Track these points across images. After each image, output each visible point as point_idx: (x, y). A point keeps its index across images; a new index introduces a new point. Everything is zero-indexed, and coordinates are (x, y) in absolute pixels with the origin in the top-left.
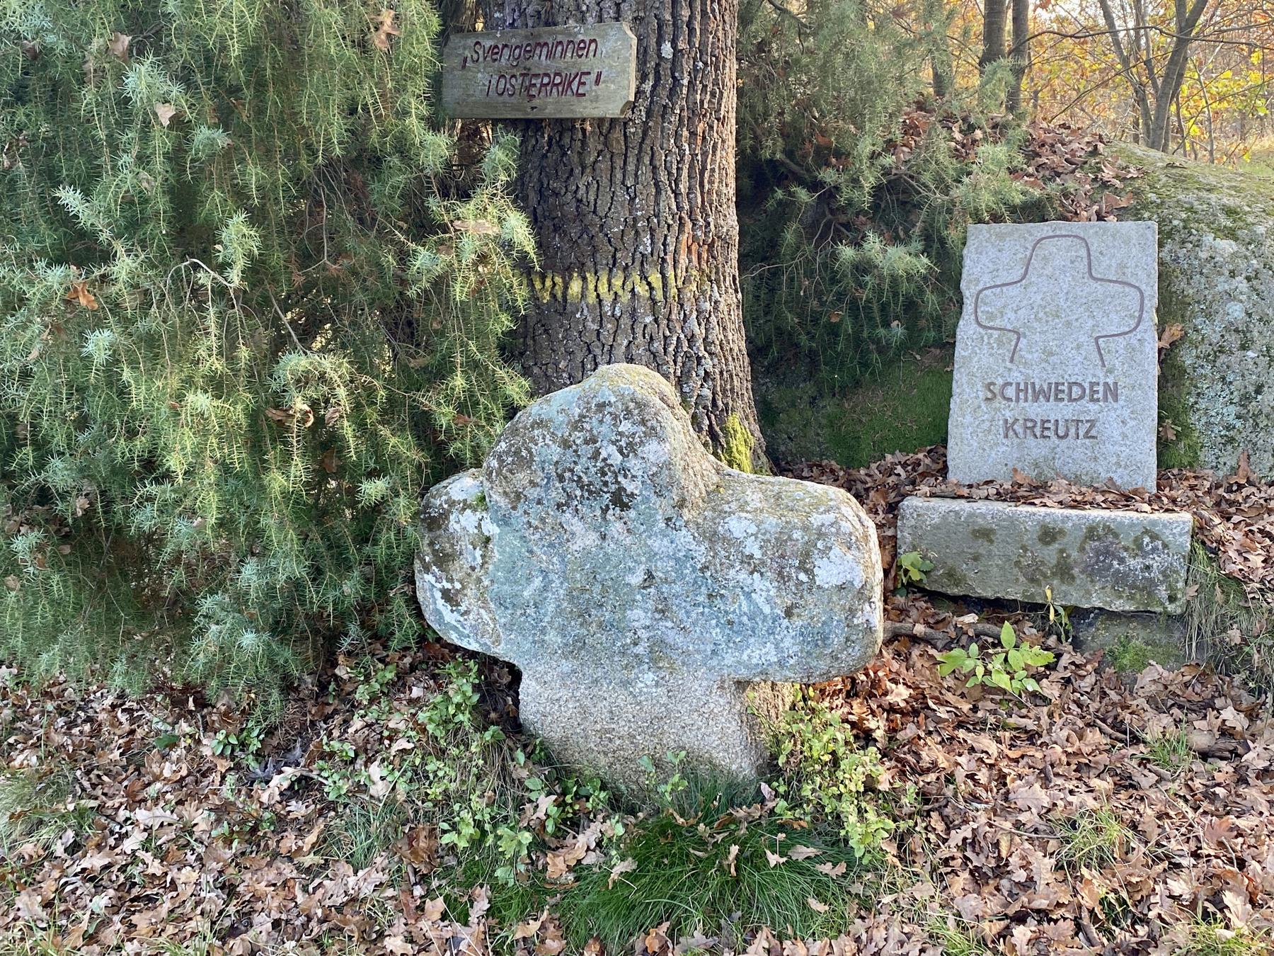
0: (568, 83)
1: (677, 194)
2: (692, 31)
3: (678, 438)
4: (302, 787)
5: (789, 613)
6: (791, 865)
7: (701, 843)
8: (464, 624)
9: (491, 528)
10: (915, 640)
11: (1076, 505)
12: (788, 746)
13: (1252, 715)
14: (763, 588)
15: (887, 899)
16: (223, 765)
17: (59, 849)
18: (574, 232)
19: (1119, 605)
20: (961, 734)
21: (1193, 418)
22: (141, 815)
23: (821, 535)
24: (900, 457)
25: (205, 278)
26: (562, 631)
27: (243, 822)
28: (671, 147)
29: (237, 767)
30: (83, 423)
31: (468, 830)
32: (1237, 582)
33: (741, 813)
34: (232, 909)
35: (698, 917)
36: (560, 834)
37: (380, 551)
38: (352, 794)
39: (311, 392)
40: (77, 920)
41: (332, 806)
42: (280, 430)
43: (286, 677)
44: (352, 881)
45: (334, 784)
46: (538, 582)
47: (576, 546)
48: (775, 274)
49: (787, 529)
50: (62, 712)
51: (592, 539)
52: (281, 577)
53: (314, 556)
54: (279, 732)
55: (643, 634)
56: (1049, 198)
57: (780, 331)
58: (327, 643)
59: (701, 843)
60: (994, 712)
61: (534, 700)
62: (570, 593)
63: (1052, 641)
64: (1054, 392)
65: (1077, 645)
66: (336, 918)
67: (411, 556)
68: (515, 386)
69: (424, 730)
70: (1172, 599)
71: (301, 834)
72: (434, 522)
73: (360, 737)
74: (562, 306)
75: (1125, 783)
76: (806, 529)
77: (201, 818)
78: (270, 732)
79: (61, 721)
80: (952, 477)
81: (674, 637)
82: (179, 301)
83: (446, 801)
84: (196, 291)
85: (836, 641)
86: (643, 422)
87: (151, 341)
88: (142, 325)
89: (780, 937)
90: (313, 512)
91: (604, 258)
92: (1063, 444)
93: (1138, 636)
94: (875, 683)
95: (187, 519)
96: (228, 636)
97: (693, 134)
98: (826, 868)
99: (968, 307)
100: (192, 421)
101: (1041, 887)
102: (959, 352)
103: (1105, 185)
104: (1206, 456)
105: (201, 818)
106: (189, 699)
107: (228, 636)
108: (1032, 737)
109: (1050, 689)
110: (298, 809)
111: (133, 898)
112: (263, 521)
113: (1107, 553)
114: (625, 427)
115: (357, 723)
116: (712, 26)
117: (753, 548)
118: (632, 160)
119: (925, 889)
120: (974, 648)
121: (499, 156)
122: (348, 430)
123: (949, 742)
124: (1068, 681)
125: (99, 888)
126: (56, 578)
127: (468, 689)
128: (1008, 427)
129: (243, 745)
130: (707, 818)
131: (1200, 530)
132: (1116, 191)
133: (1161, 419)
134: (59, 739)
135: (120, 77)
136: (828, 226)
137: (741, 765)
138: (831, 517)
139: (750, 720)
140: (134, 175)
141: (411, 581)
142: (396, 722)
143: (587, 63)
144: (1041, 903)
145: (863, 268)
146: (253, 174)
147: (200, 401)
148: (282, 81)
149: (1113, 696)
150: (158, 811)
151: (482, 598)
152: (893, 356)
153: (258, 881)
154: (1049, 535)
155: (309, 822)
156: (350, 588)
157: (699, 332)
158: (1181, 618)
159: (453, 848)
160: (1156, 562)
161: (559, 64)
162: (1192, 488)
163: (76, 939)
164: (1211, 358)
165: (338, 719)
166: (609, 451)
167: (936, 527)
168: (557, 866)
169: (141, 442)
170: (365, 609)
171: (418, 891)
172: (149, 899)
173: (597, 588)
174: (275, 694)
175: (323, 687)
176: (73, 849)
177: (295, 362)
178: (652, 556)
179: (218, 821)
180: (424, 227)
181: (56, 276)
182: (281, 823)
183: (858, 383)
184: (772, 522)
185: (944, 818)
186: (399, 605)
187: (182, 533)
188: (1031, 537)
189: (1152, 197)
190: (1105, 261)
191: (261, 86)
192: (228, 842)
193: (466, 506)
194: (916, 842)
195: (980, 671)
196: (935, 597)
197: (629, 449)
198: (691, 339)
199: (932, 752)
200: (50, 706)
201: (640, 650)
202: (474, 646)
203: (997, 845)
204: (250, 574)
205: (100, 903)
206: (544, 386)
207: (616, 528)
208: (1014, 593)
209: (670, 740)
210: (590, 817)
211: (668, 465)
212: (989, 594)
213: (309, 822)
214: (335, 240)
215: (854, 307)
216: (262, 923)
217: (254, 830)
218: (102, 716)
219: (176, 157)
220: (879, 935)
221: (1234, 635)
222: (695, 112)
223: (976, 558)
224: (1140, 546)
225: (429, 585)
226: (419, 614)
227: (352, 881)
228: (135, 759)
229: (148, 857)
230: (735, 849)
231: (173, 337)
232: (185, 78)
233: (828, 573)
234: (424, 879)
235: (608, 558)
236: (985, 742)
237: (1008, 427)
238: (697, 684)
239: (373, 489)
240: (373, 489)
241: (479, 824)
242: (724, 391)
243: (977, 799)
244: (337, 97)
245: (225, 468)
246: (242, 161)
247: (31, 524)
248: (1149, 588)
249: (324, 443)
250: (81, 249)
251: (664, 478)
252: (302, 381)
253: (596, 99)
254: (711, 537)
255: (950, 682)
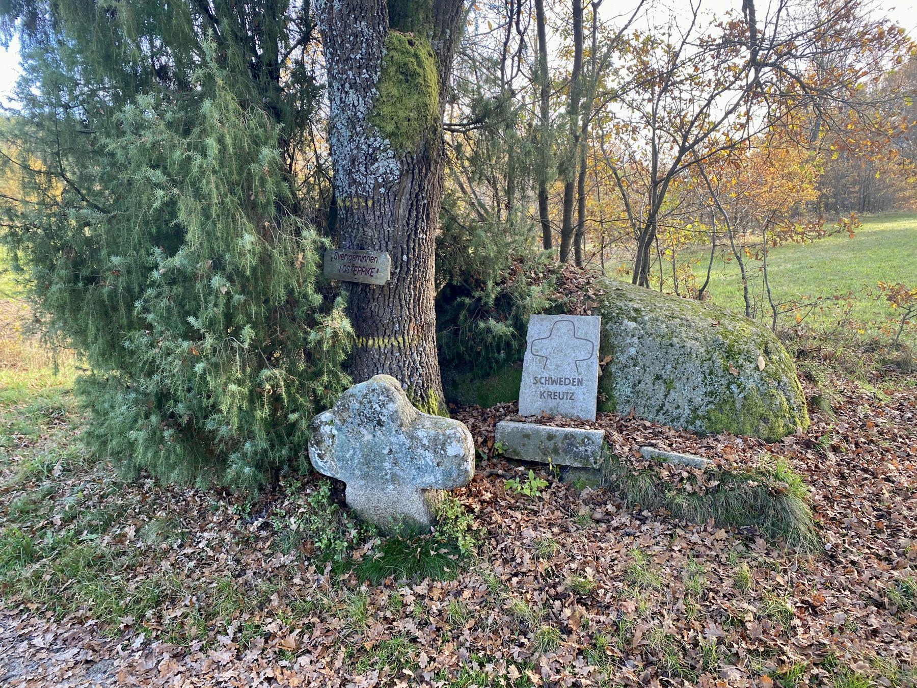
0: (368, 271)
1: (409, 309)
2: (414, 251)
3: (401, 402)
4: (265, 526)
5: (438, 465)
6: (438, 555)
7: (408, 548)
8: (326, 466)
9: (335, 432)
10: (498, 476)
11: (563, 426)
12: (440, 513)
13: (618, 507)
14: (429, 455)
15: (472, 568)
16: (236, 517)
17: (175, 547)
18: (370, 322)
19: (576, 465)
20: (509, 511)
21: (615, 392)
22: (205, 534)
23: (449, 437)
24: (503, 404)
25: (236, 345)
26: (360, 470)
27: (243, 538)
28: (407, 292)
29: (241, 518)
30: (189, 390)
31: (325, 541)
32: (616, 457)
33: (422, 537)
34: (239, 568)
35: (405, 573)
36: (358, 544)
37: (296, 439)
38: (283, 528)
39: (271, 383)
40: (183, 570)
41: (276, 533)
42: (261, 395)
43: (260, 485)
44: (282, 559)
45: (277, 524)
46: (351, 452)
47: (365, 439)
48: (456, 331)
49: (438, 435)
50: (173, 497)
51: (370, 437)
52: (260, 448)
53: (271, 440)
54: (257, 506)
55: (389, 471)
56: (565, 303)
57: (458, 354)
58: (275, 471)
59: (408, 548)
60: (523, 504)
61: (351, 495)
62: (363, 456)
63: (550, 478)
64: (559, 381)
65: (561, 480)
66: (276, 572)
67: (307, 441)
68: (345, 379)
69: (310, 505)
70: (595, 463)
71: (264, 542)
72: (315, 429)
73: (287, 508)
74: (365, 349)
75: (565, 530)
76: (444, 435)
77: (228, 536)
78: (254, 505)
79: (173, 500)
80: (520, 413)
81: (399, 473)
82: (226, 351)
83: (317, 532)
84: (232, 348)
85: (455, 475)
86: (388, 396)
87: (216, 365)
88: (213, 359)
89: (433, 581)
90: (272, 424)
91: (381, 332)
92: (562, 401)
93: (583, 476)
94: (479, 492)
95: (225, 423)
96: (239, 469)
97: (415, 287)
98: (451, 557)
99: (529, 347)
100: (231, 394)
101: (525, 565)
102: (525, 364)
103: (589, 297)
104: (619, 407)
105: (228, 536)
106: (223, 492)
107: (239, 469)
108: (535, 513)
109: (546, 496)
110: (263, 533)
111: (203, 563)
112: (253, 428)
113: (572, 445)
114: (381, 398)
115: (287, 503)
116: (422, 248)
117: (426, 442)
118: (392, 297)
119: (485, 565)
120: (518, 479)
121: (341, 302)
122: (284, 396)
123: (503, 515)
124: (554, 493)
125: (191, 560)
126: (178, 446)
127: (327, 490)
128: (542, 394)
129: (244, 510)
130: (411, 538)
131: (607, 437)
132: (593, 300)
133: (599, 392)
134: (172, 507)
135: (209, 279)
136: (479, 311)
137: (424, 520)
138: (453, 431)
139: (427, 504)
140: (213, 311)
141: (307, 450)
142: (301, 502)
143: (374, 265)
144: (524, 570)
145: (489, 330)
146: (253, 309)
147: (233, 387)
148: (264, 277)
149: (571, 499)
150: (212, 533)
151: (331, 457)
152: (500, 365)
153: (248, 559)
154: (551, 437)
155: (267, 538)
156: (284, 452)
157: (417, 358)
158: (599, 470)
159: (319, 548)
160: (589, 448)
161: (364, 264)
162: (610, 420)
163: (183, 577)
164: (622, 369)
165: (280, 501)
166: (376, 406)
167: (510, 433)
168: (357, 555)
169: (211, 401)
170: (290, 460)
171: (306, 563)
172: (209, 564)
173: (372, 455)
174: (256, 491)
175: (274, 489)
176: (181, 546)
177: (266, 373)
178: (391, 443)
179: (234, 537)
180: (313, 324)
181: (186, 344)
182: (257, 538)
183: (489, 374)
184: (432, 432)
185: (497, 541)
186: (302, 458)
187: (223, 430)
188: (544, 438)
189: (607, 303)
190: (580, 331)
191: (256, 279)
192: (238, 544)
193: (327, 423)
194: (485, 549)
195: (519, 488)
196: (509, 460)
197: (383, 406)
198: (414, 362)
199: (496, 517)
200: (169, 494)
201: (388, 477)
202: (329, 475)
203: (513, 550)
204: (248, 446)
205: (192, 564)
206: (355, 382)
207: (379, 433)
208: (538, 459)
209: (399, 510)
210: (369, 538)
211: (396, 411)
212: (528, 459)
213: (267, 538)
214: (280, 326)
215: (486, 347)
216: (250, 573)
217: (247, 541)
218: (189, 499)
219: (227, 304)
220: (467, 580)
221: (614, 477)
222: (416, 279)
223: (524, 445)
224: (584, 443)
225: (313, 452)
226: (310, 463)
227: (282, 559)
228: (203, 514)
229: (208, 549)
230: (419, 549)
231: (224, 364)
232: (230, 278)
233: (451, 451)
234: (308, 559)
235: (376, 444)
236: (518, 515)
237: (542, 394)
238: (408, 490)
239: (293, 417)
240: (293, 417)
241: (329, 540)
242: (427, 381)
243: (510, 534)
244: (283, 284)
245: (240, 408)
246: (249, 305)
247: (168, 426)
248: (587, 458)
249: (276, 399)
250: (194, 335)
251: (395, 416)
252: (269, 379)
253: (377, 278)
254: (412, 437)
255: (509, 492)
